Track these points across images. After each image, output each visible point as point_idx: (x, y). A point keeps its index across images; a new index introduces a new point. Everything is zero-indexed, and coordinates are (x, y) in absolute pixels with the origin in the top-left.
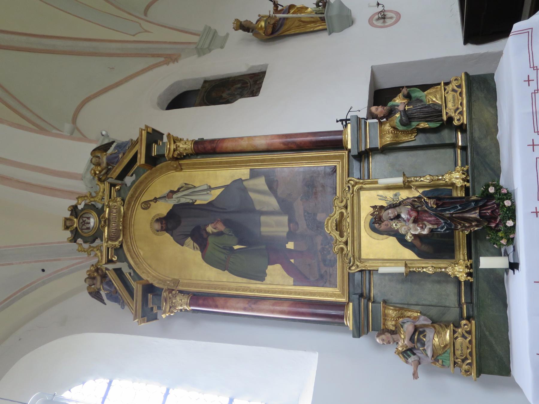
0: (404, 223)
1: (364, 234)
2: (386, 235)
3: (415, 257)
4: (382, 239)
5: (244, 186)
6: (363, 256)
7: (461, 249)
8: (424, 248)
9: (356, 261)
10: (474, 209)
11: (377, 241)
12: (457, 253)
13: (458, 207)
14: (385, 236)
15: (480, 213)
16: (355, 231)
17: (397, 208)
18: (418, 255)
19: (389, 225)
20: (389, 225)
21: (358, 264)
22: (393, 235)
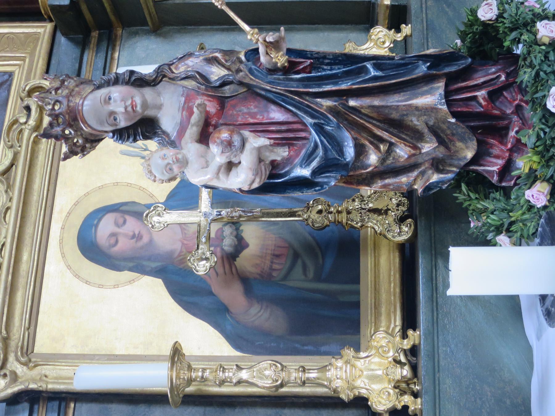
0: (162, 144)
1: (54, 266)
2: (131, 269)
3: (225, 349)
4: (116, 286)
5: (21, 402)
6: (43, 345)
7: (383, 318)
8: (259, 316)
9: (11, 358)
10: (428, 79)
11: (95, 291)
12: (366, 329)
13: (367, 71)
14: (127, 275)
15: (448, 94)
16: (25, 256)
17: (148, 92)
18: (237, 340)
19: (145, 239)
20: (145, 239)
21: (20, 370)
22: (157, 273)
